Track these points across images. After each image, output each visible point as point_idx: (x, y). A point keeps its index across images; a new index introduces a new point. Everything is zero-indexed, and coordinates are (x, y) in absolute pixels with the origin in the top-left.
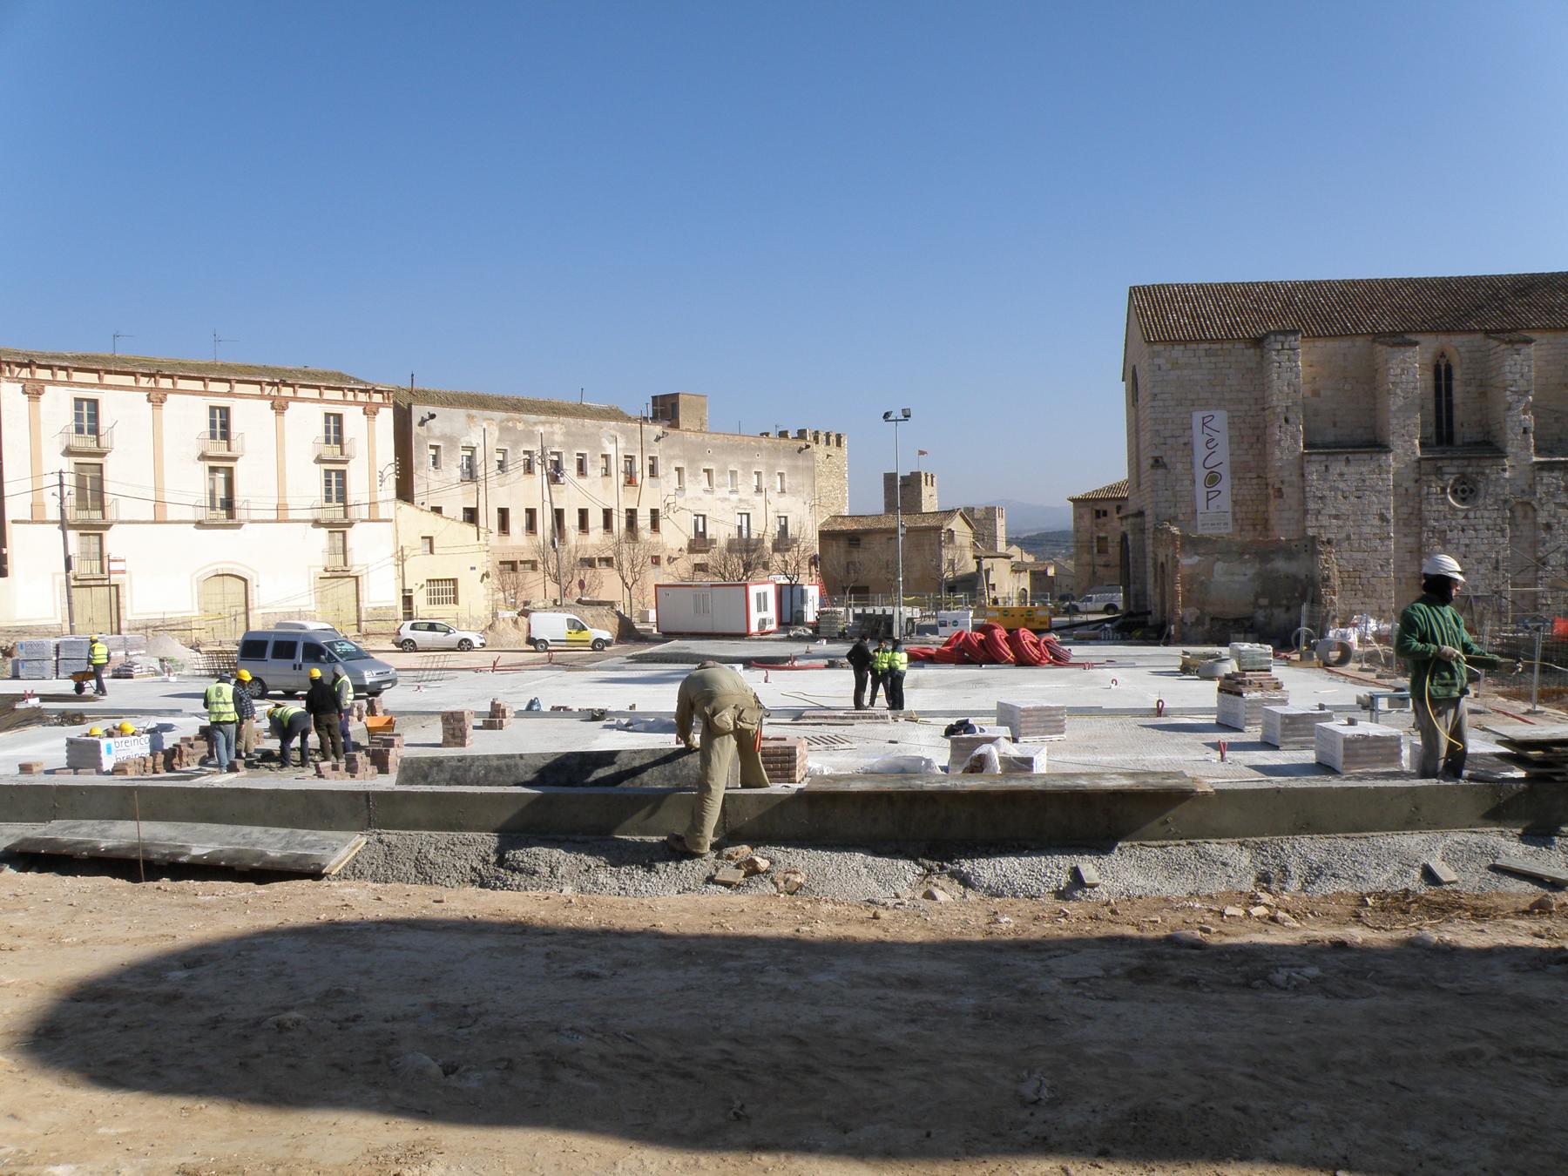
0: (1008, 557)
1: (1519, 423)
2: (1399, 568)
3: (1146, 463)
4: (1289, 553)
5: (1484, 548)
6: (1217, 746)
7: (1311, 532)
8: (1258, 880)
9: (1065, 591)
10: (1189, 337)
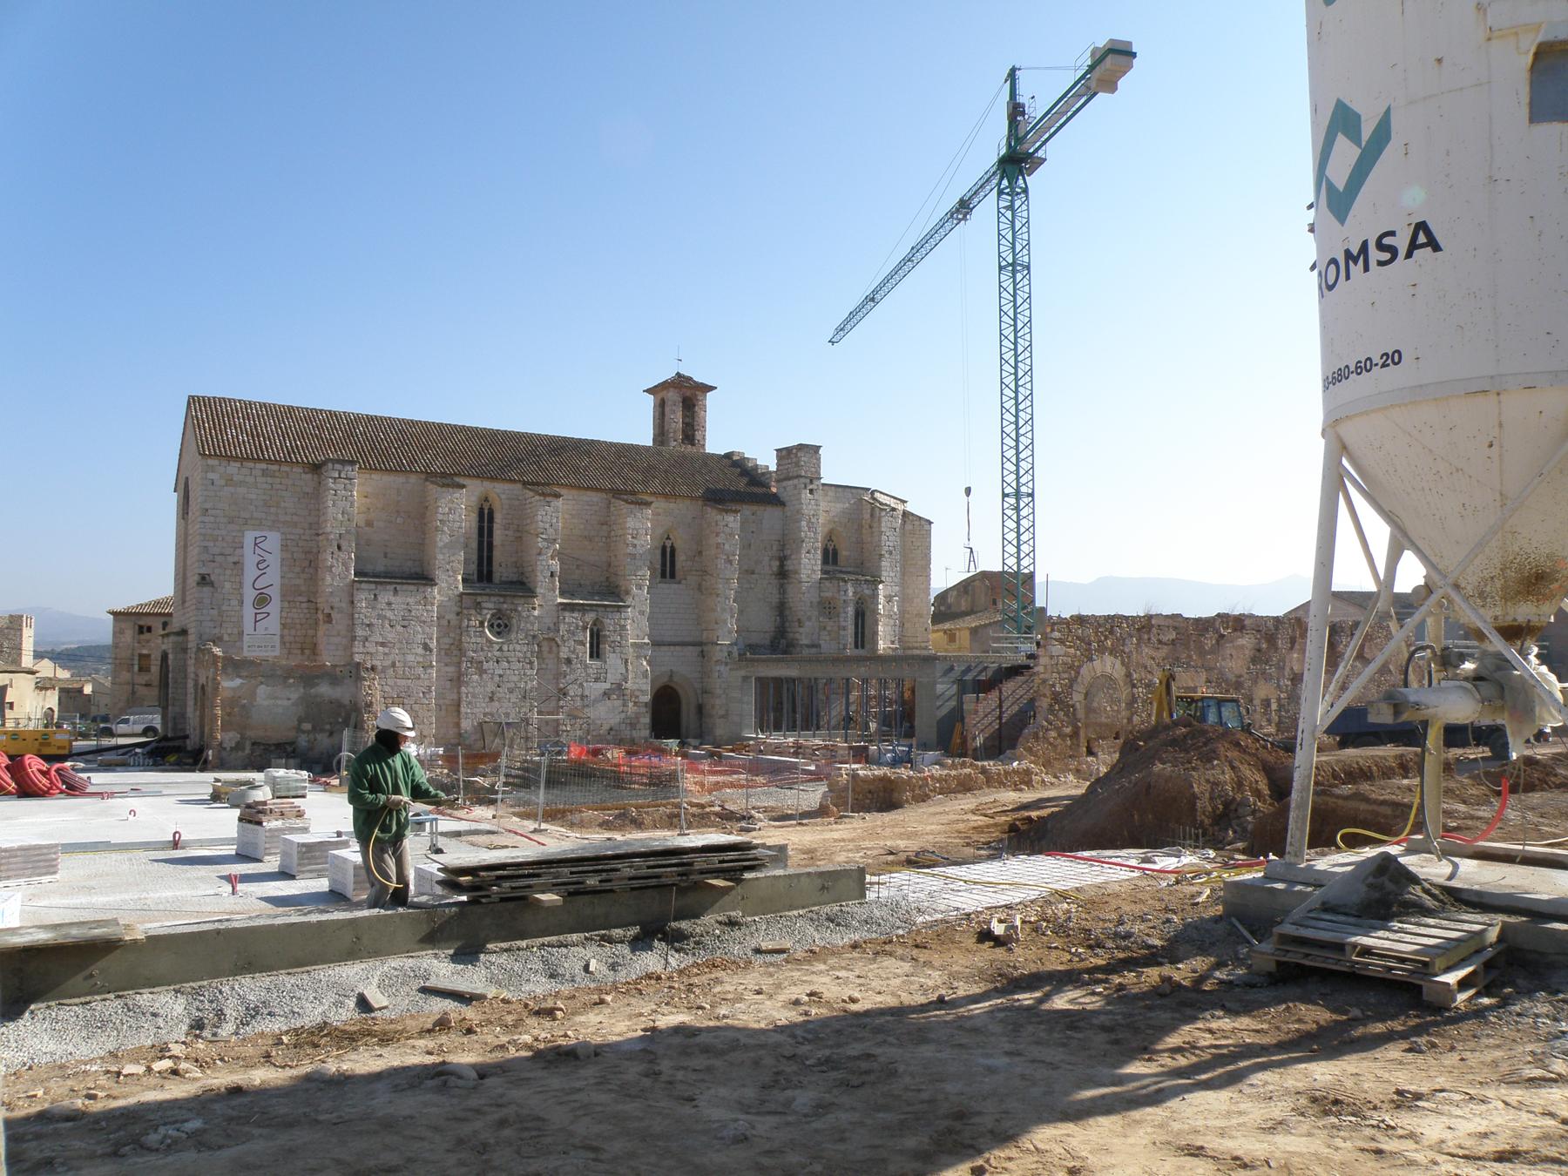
0: (33, 673)
1: (547, 567)
2: (439, 696)
3: (193, 580)
4: (334, 678)
5: (515, 679)
6: (229, 879)
7: (357, 658)
8: (192, 1027)
9: (103, 711)
10: (244, 454)
